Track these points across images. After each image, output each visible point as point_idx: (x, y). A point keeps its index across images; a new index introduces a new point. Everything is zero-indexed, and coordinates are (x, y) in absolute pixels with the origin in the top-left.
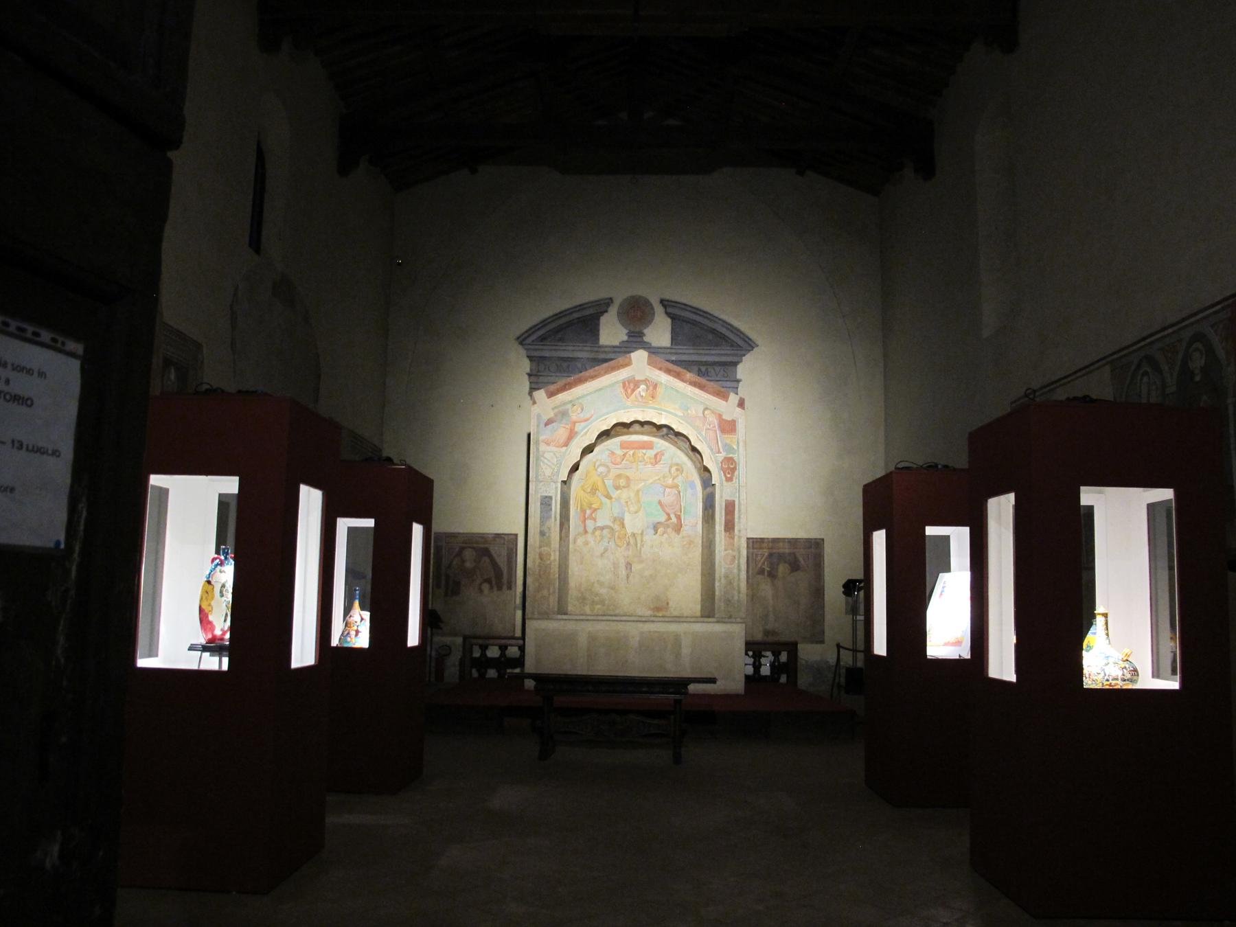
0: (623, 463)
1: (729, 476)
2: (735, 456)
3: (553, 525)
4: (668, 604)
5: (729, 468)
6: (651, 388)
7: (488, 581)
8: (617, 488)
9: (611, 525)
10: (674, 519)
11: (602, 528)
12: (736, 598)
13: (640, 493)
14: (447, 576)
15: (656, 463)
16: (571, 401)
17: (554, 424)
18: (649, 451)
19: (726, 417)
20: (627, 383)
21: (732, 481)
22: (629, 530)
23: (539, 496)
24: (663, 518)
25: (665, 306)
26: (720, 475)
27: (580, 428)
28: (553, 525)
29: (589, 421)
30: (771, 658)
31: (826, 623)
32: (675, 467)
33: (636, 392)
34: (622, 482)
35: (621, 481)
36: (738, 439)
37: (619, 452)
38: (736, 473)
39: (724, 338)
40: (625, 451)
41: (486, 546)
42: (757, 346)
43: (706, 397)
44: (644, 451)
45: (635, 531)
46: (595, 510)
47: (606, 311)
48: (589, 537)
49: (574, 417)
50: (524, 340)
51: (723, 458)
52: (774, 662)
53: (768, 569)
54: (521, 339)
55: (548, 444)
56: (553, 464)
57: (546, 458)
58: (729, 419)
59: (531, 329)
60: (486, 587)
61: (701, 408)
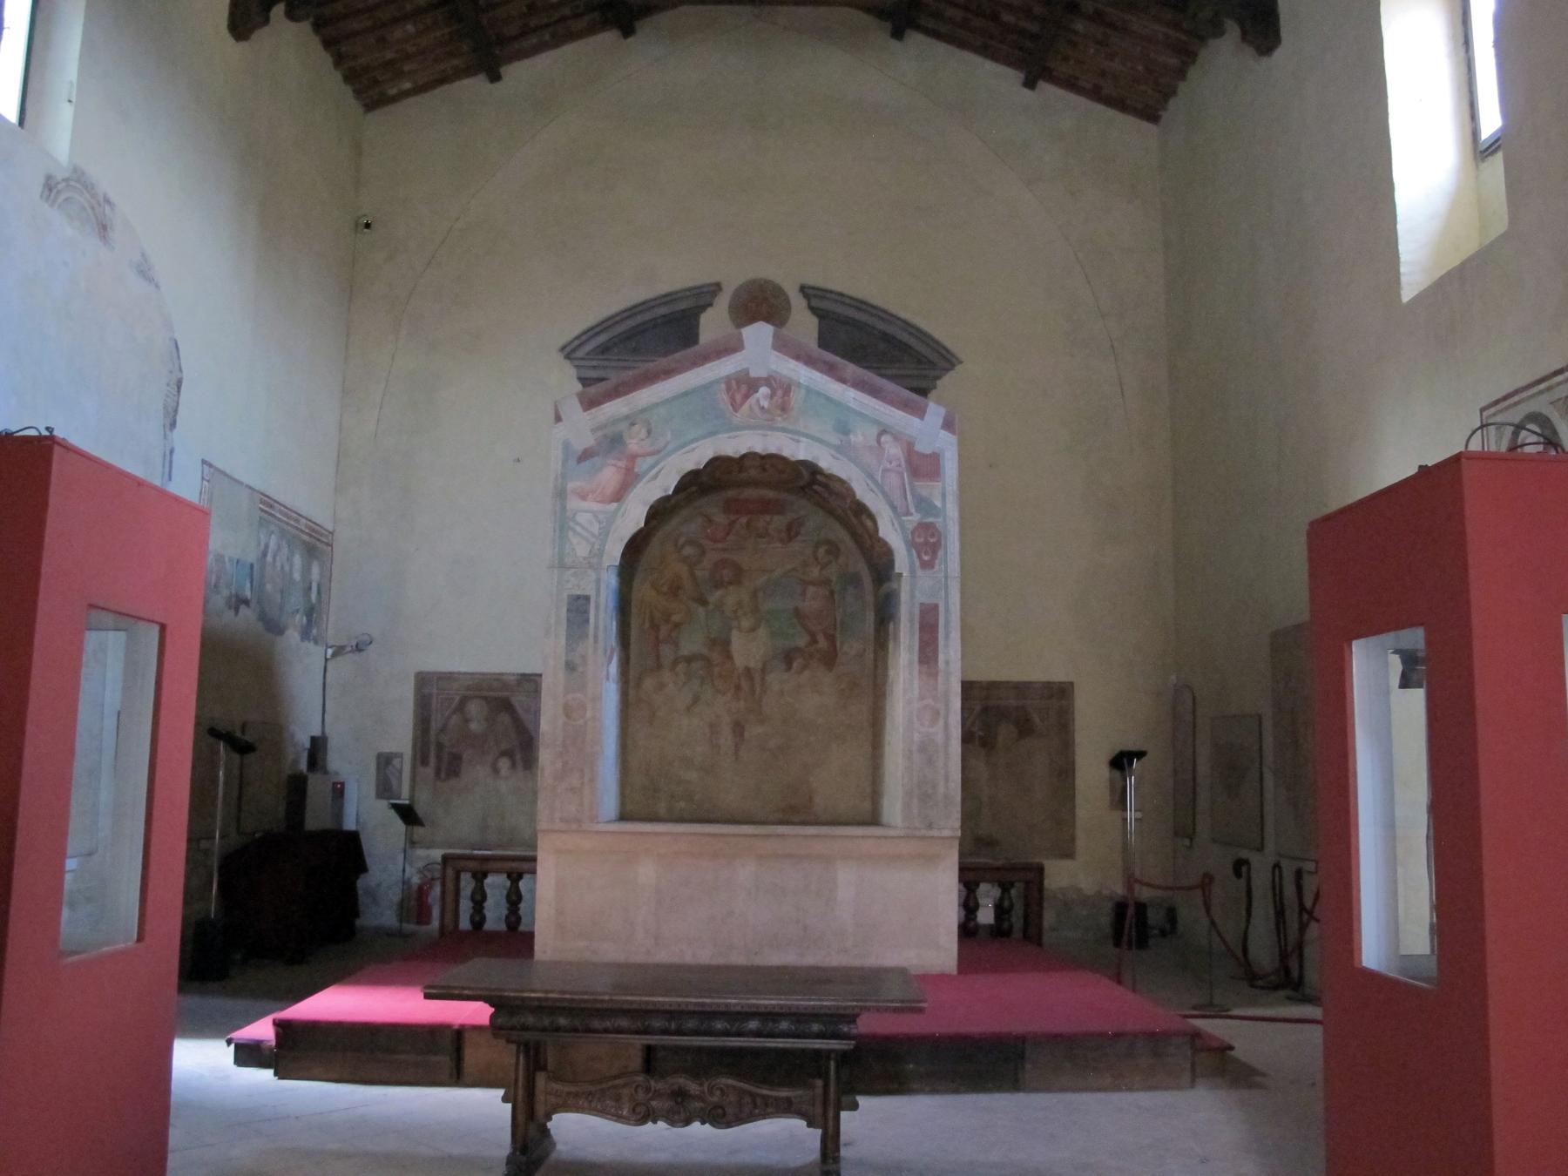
0: (728, 538)
1: (926, 558)
2: (939, 521)
3: (590, 651)
4: (811, 799)
5: (926, 543)
6: (780, 393)
7: (508, 754)
8: (718, 584)
9: (705, 651)
10: (823, 643)
11: (689, 660)
12: (941, 789)
13: (761, 594)
14: (440, 746)
15: (790, 539)
16: (627, 417)
17: (596, 458)
18: (776, 518)
19: (922, 447)
20: (734, 382)
21: (933, 567)
22: (739, 661)
23: (565, 595)
24: (802, 641)
25: (807, 296)
26: (910, 555)
27: (645, 466)
28: (590, 651)
29: (662, 454)
30: (996, 892)
31: (1079, 823)
32: (826, 547)
33: (752, 400)
34: (727, 574)
35: (725, 572)
36: (944, 488)
37: (721, 519)
38: (941, 553)
39: (905, 348)
40: (732, 517)
41: (506, 694)
42: (961, 362)
43: (882, 409)
44: (768, 518)
45: (752, 665)
46: (677, 625)
47: (710, 305)
48: (666, 676)
49: (633, 445)
50: (574, 351)
51: (915, 524)
52: (1001, 899)
53: (981, 733)
54: (568, 349)
55: (583, 497)
56: (593, 535)
57: (578, 524)
58: (928, 451)
59: (585, 333)
60: (504, 764)
61: (874, 431)
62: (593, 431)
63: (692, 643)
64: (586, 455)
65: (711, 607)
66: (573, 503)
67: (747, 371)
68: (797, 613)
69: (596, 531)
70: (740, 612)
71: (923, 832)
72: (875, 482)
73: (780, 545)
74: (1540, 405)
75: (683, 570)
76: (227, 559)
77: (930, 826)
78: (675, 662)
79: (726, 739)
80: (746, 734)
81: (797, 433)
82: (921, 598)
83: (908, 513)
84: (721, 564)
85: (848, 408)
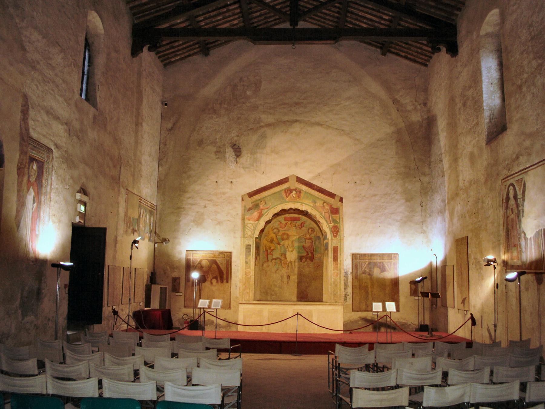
3: (251, 259)
5: (335, 231)
6: (298, 193)
7: (216, 278)
8: (283, 239)
9: (280, 257)
10: (310, 255)
11: (276, 259)
15: (301, 228)
16: (260, 199)
19: (334, 206)
22: (289, 260)
23: (245, 245)
24: (305, 254)
28: (251, 259)
33: (291, 195)
34: (285, 237)
37: (284, 222)
38: (339, 233)
40: (287, 222)
44: (296, 222)
45: (292, 260)
48: (270, 263)
49: (261, 207)
55: (249, 220)
56: (252, 229)
57: (248, 227)
60: (214, 281)
61: (322, 202)
62: (252, 203)
63: (276, 254)
64: (250, 209)
65: (281, 245)
66: (247, 221)
67: (289, 187)
68: (303, 247)
69: (252, 228)
70: (289, 247)
71: (334, 304)
72: (322, 215)
73: (299, 229)
74: (512, 181)
75: (274, 236)
76: (131, 218)
77: (336, 302)
78: (272, 259)
79: (285, 280)
80: (290, 278)
81: (303, 203)
82: (334, 245)
83: (331, 223)
84: (284, 234)
85: (315, 197)
